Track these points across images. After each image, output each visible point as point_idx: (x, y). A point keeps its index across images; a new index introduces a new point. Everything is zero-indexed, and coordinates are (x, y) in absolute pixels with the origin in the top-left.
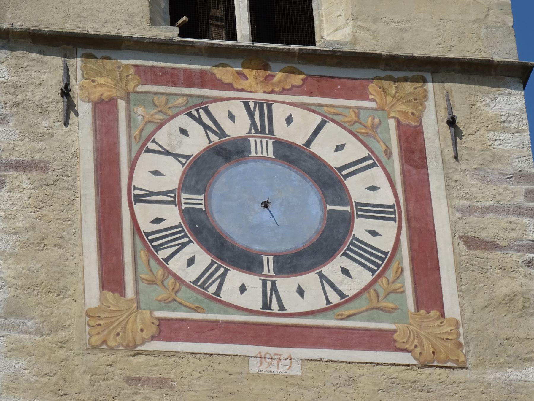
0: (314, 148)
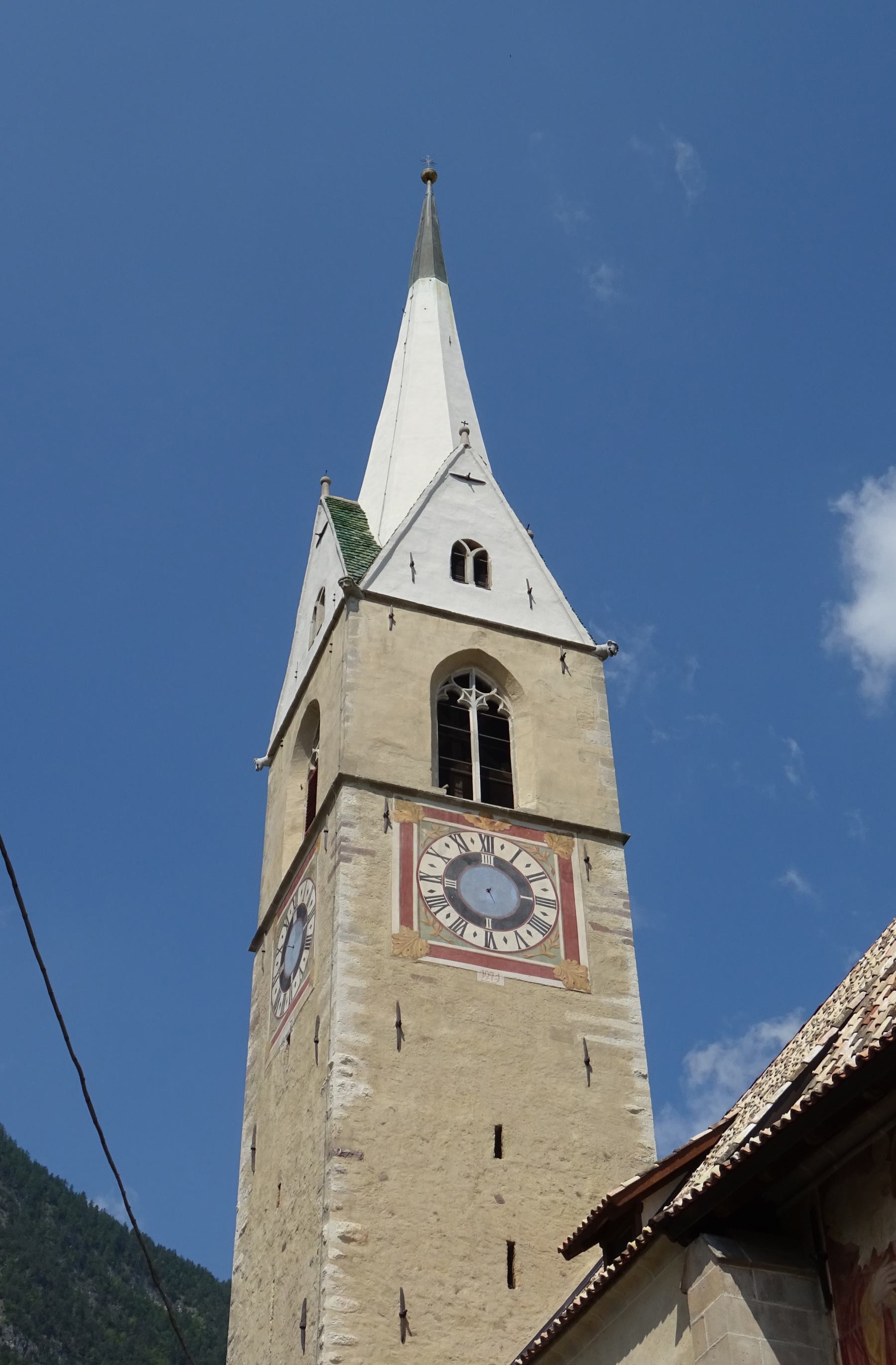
0: (514, 864)
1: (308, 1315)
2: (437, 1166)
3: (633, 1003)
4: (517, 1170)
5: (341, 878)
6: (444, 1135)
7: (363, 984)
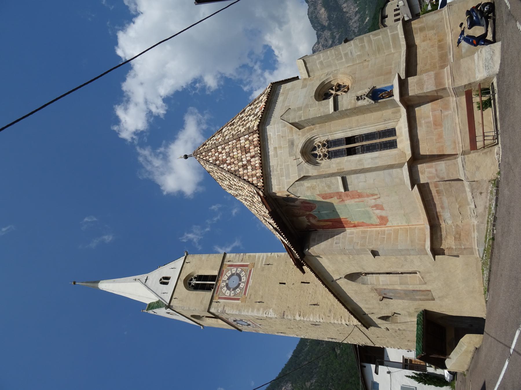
1: (314, 324)
2: (287, 296)
3: (257, 254)
5: (229, 312)
7: (251, 309)
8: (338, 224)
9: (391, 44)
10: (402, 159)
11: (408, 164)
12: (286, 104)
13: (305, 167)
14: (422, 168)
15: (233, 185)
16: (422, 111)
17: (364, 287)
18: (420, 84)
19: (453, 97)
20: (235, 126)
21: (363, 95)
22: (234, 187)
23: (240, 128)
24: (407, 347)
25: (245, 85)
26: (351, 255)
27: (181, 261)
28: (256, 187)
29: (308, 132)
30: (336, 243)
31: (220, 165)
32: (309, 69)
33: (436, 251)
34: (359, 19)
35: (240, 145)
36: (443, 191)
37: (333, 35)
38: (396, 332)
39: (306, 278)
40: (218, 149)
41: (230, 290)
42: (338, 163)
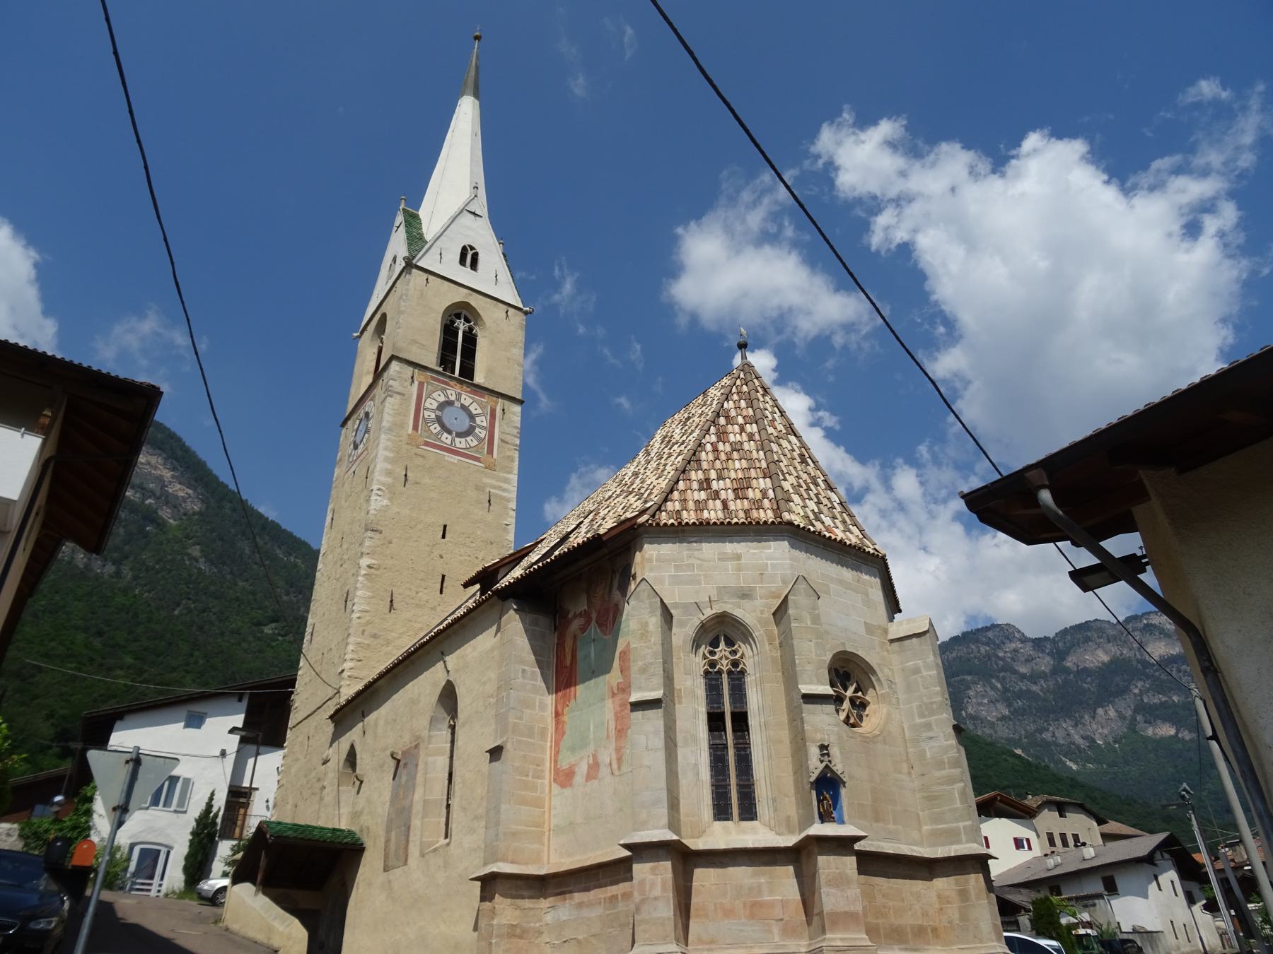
0: (470, 408)
1: (349, 597)
2: (415, 539)
3: (514, 477)
4: (450, 545)
6: (420, 527)
7: (391, 455)
8: (565, 681)
9: (940, 827)
10: (689, 829)
11: (674, 841)
12: (833, 587)
13: (691, 619)
14: (665, 869)
15: (670, 449)
16: (784, 881)
17: (424, 722)
18: (839, 881)
19: (808, 947)
20: (797, 465)
21: (830, 759)
22: (666, 450)
23: (791, 479)
24: (282, 801)
25: (930, 449)
26: (497, 700)
27: (512, 297)
28: (659, 509)
29: (766, 633)
30: (524, 671)
31: (715, 426)
32: (907, 642)
33: (490, 884)
34: (1074, 743)
35: (754, 478)
36: (614, 909)
37: (1041, 677)
38: (319, 780)
39: (453, 586)
40: (751, 424)
41: (438, 409)
42: (693, 692)
